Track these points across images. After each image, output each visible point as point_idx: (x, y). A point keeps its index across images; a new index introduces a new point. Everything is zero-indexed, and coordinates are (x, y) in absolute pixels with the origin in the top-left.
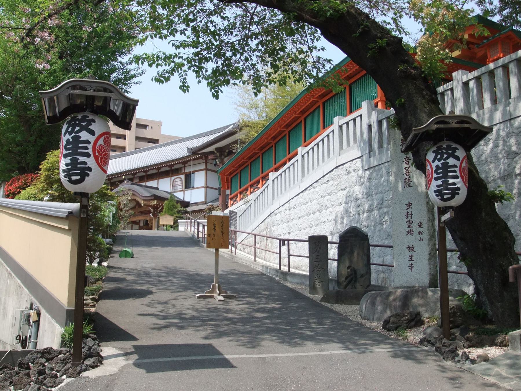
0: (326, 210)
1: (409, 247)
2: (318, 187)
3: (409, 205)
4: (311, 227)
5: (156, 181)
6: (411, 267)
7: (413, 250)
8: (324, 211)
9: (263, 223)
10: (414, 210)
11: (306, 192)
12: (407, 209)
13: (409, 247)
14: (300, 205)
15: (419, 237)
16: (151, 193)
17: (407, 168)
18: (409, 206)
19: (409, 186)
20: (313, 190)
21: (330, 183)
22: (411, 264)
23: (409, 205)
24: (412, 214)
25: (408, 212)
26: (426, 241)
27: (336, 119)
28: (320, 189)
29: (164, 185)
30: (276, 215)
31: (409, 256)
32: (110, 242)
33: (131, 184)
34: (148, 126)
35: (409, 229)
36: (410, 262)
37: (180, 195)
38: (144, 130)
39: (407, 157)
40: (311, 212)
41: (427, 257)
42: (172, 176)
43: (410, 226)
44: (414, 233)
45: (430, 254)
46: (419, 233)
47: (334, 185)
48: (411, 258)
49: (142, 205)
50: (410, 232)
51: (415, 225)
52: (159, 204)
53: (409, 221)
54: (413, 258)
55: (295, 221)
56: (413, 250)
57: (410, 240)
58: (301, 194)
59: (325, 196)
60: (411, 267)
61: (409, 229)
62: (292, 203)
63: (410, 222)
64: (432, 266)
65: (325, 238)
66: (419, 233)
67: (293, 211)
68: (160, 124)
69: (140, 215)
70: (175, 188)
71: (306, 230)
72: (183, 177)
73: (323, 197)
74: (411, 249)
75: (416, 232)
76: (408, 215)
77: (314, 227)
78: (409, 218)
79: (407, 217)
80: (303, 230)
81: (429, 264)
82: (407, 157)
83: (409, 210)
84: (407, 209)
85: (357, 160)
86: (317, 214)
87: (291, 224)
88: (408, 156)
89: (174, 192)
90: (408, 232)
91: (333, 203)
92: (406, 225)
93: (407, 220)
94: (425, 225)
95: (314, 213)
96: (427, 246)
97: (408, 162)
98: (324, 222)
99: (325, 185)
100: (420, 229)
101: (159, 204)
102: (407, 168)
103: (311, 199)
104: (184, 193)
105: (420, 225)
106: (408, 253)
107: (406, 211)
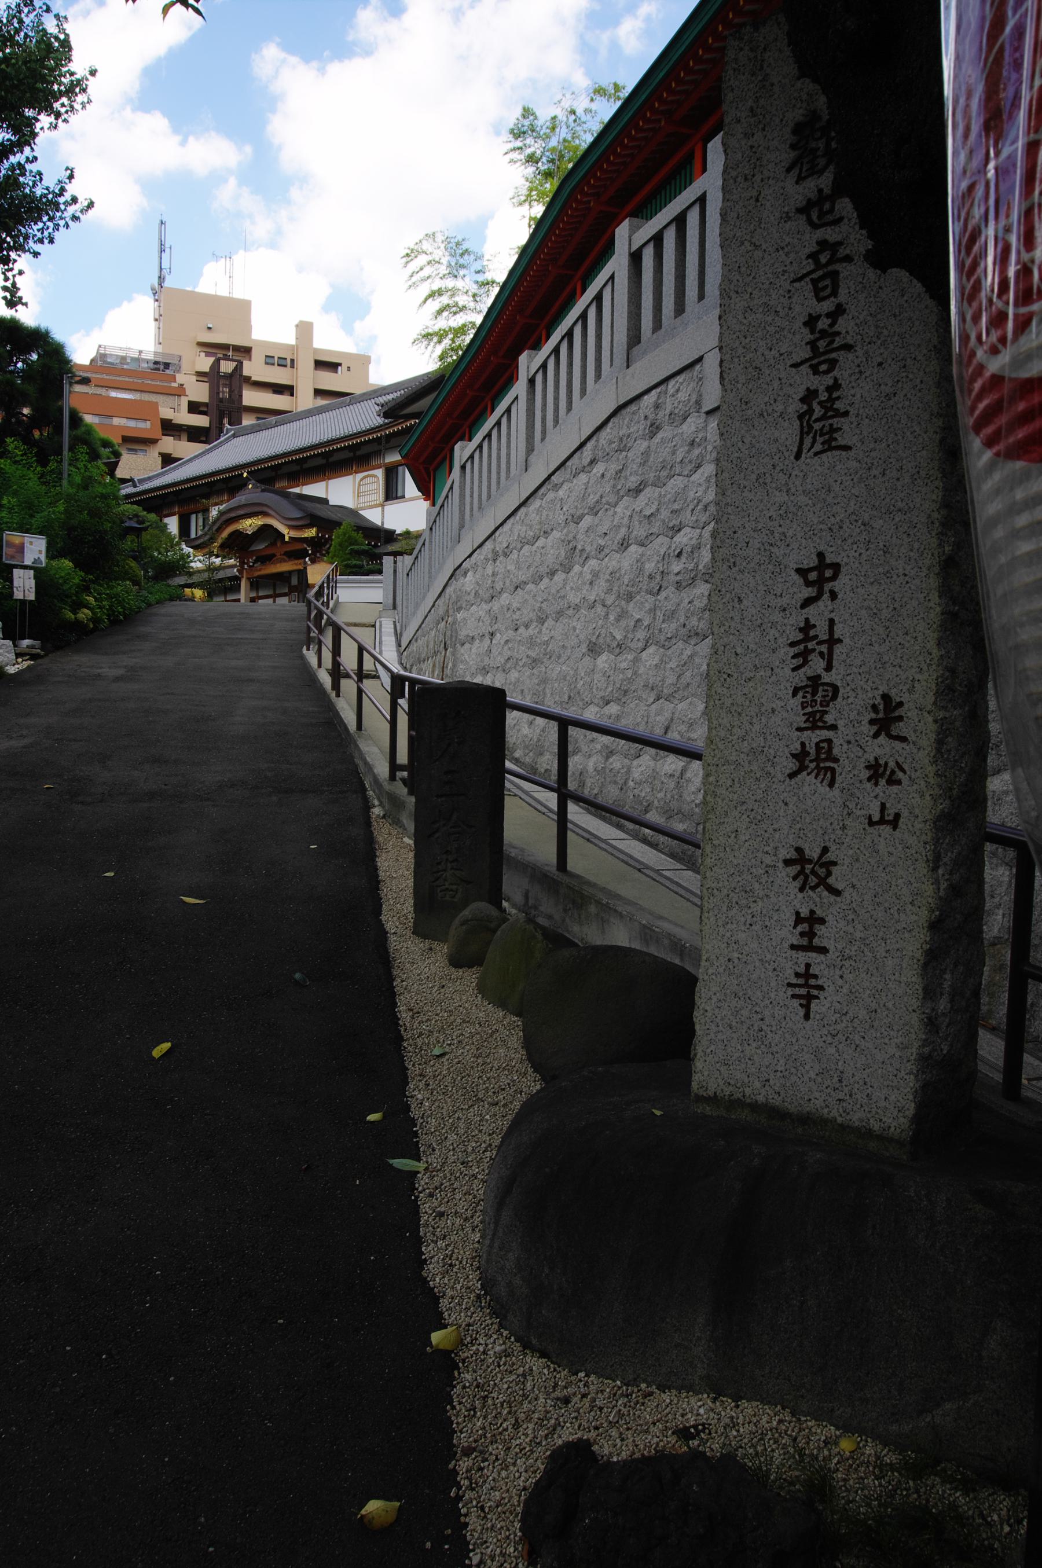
0: (583, 565)
1: (799, 859)
2: (565, 487)
3: (820, 576)
4: (542, 621)
5: (324, 483)
6: (806, 989)
7: (823, 882)
8: (577, 568)
9: (442, 599)
10: (849, 609)
11: (536, 503)
12: (807, 603)
13: (799, 859)
14: (519, 546)
15: (872, 798)
16: (303, 511)
17: (823, 324)
18: (820, 582)
19: (830, 446)
20: (551, 495)
21: (599, 469)
22: (807, 975)
23: (820, 576)
24: (832, 641)
25: (807, 627)
26: (915, 835)
27: (622, 232)
28: (571, 490)
29: (340, 492)
30: (466, 574)
31: (799, 919)
32: (33, 647)
33: (263, 491)
34: (340, 364)
35: (812, 738)
36: (803, 957)
37: (373, 516)
38: (332, 375)
39: (823, 244)
40: (544, 570)
41: (914, 944)
42: (356, 473)
43: (814, 721)
44: (843, 769)
45: (934, 926)
46: (876, 771)
47: (608, 476)
48: (810, 934)
49: (287, 539)
50: (816, 761)
51: (851, 715)
52: (323, 536)
53: (815, 681)
54: (825, 935)
55: (505, 599)
56: (823, 882)
57: (814, 811)
58: (523, 510)
59: (581, 518)
60: (806, 989)
61: (812, 738)
62: (503, 538)
63: (817, 696)
64: (943, 1004)
65: (501, 693)
66: (876, 771)
67: (501, 565)
68: (364, 361)
69: (285, 561)
70: (367, 499)
71: (531, 631)
72: (380, 473)
73: (577, 520)
74: (812, 870)
75: (851, 767)
76: (811, 644)
77: (550, 622)
78: (817, 665)
79: (804, 656)
80: (522, 630)
81: (929, 993)
82: (823, 244)
83: (819, 614)
84: (807, 603)
85: (680, 378)
86: (560, 577)
87: (496, 605)
88: (831, 234)
89: (362, 509)
90: (800, 757)
91: (601, 542)
92: (793, 710)
93: (800, 679)
94: (920, 724)
95: (552, 573)
96: (922, 868)
97: (834, 276)
98: (577, 608)
99: (583, 477)
100: (882, 748)
101: (323, 536)
102: (823, 324)
103: (546, 527)
104: (383, 511)
105: (886, 717)
106: (789, 899)
107: (797, 619)
